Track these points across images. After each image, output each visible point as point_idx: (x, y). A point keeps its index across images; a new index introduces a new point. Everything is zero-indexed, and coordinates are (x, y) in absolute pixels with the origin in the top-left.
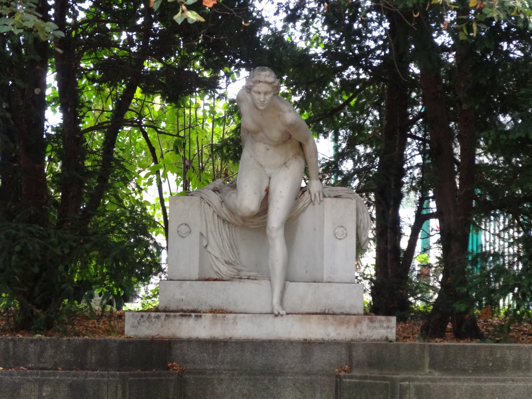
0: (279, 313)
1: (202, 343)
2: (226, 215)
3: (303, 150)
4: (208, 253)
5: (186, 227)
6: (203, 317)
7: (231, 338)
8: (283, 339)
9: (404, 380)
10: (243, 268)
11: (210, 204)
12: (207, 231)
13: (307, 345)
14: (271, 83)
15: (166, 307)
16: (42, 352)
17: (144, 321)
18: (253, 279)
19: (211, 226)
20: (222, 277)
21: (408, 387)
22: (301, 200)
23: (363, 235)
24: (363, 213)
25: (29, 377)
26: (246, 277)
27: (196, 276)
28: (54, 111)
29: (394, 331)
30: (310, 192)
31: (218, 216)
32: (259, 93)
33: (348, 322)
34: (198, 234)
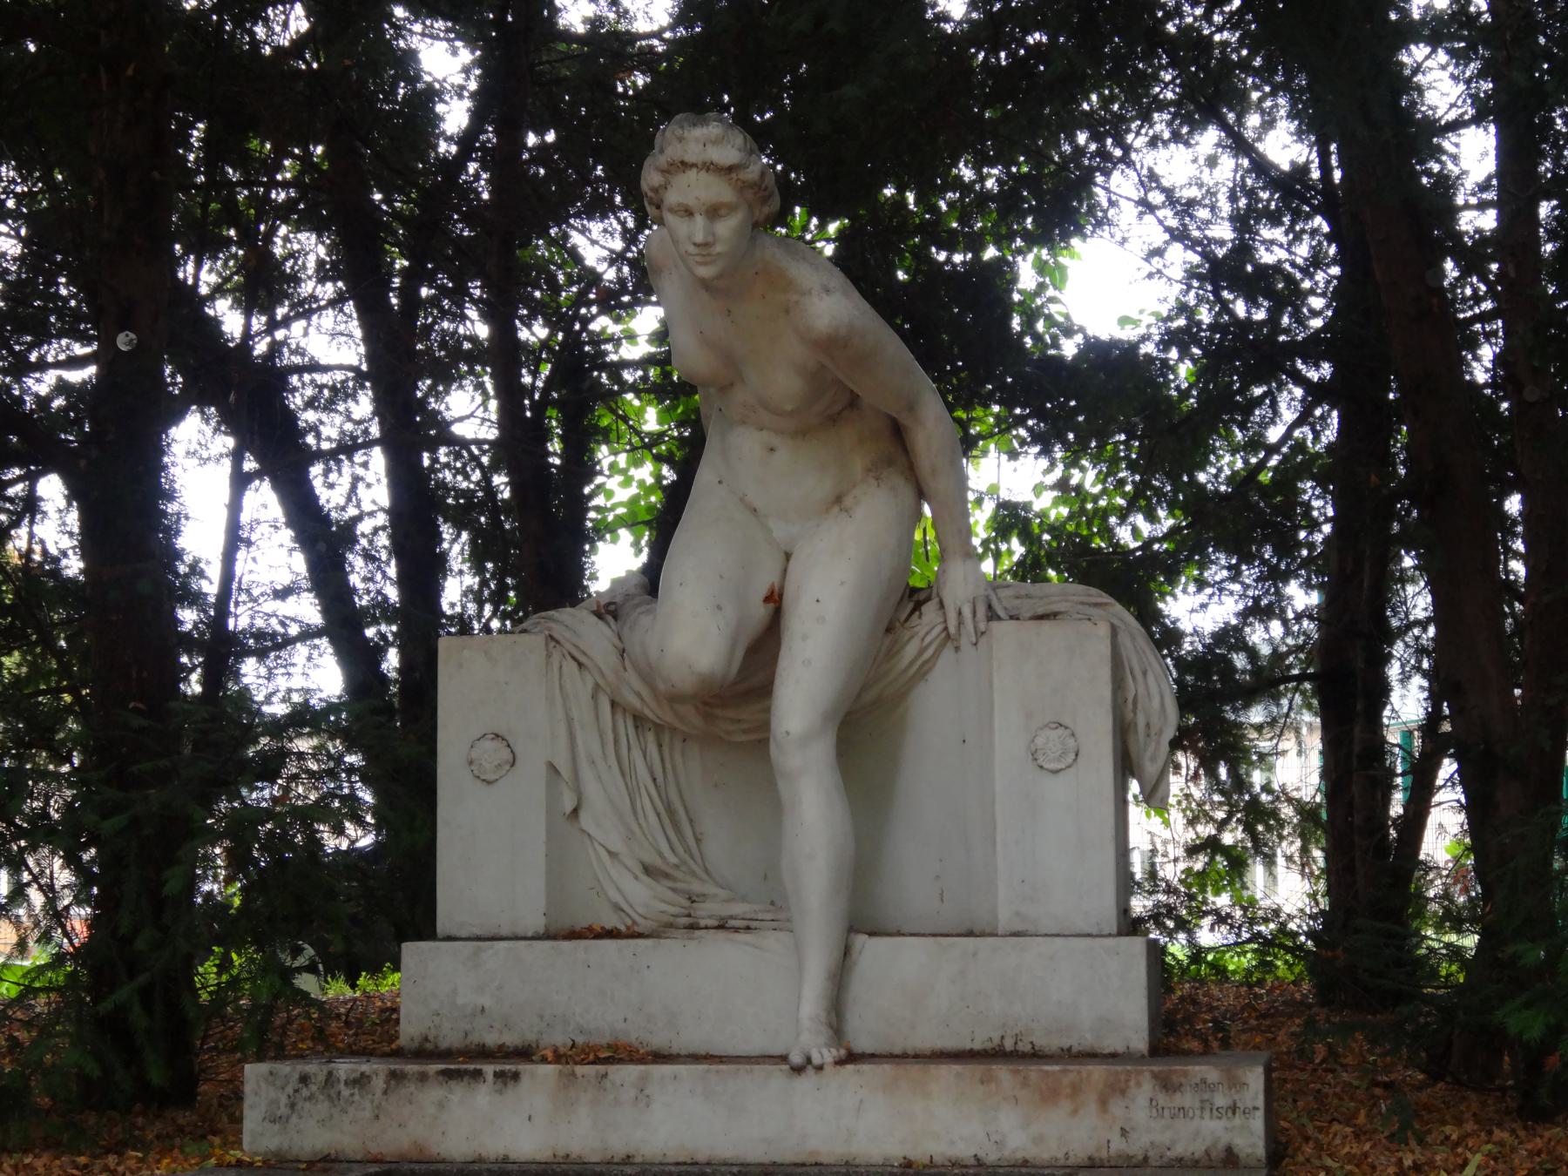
0: (809, 1060)
2: (639, 695)
6: (525, 1081)
8: (825, 1160)
10: (710, 889)
11: (582, 659)
14: (730, 169)
15: (426, 1039)
17: (310, 1098)
19: (588, 742)
20: (634, 922)
22: (908, 634)
23: (1149, 754)
24: (1145, 673)
26: (715, 923)
27: (534, 921)
28: (636, 545)
29: (1258, 1123)
30: (942, 605)
31: (614, 704)
32: (689, 213)
33: (1076, 1090)
34: (542, 770)
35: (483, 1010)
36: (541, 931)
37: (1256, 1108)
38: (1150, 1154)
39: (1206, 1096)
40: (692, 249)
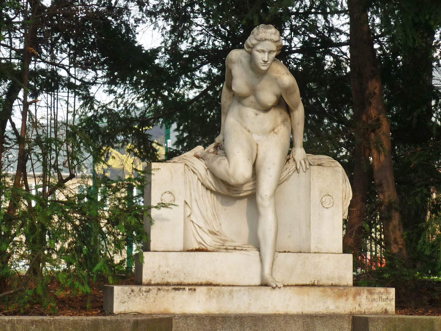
0: (277, 286)
2: (210, 181)
3: (290, 117)
4: (191, 223)
5: (169, 195)
7: (287, 314)
11: (195, 171)
14: (277, 42)
26: (233, 248)
27: (180, 246)
30: (294, 160)
32: (264, 51)
33: (347, 294)
35: (168, 272)
36: (182, 249)
37: (393, 299)
38: (366, 311)
39: (381, 296)
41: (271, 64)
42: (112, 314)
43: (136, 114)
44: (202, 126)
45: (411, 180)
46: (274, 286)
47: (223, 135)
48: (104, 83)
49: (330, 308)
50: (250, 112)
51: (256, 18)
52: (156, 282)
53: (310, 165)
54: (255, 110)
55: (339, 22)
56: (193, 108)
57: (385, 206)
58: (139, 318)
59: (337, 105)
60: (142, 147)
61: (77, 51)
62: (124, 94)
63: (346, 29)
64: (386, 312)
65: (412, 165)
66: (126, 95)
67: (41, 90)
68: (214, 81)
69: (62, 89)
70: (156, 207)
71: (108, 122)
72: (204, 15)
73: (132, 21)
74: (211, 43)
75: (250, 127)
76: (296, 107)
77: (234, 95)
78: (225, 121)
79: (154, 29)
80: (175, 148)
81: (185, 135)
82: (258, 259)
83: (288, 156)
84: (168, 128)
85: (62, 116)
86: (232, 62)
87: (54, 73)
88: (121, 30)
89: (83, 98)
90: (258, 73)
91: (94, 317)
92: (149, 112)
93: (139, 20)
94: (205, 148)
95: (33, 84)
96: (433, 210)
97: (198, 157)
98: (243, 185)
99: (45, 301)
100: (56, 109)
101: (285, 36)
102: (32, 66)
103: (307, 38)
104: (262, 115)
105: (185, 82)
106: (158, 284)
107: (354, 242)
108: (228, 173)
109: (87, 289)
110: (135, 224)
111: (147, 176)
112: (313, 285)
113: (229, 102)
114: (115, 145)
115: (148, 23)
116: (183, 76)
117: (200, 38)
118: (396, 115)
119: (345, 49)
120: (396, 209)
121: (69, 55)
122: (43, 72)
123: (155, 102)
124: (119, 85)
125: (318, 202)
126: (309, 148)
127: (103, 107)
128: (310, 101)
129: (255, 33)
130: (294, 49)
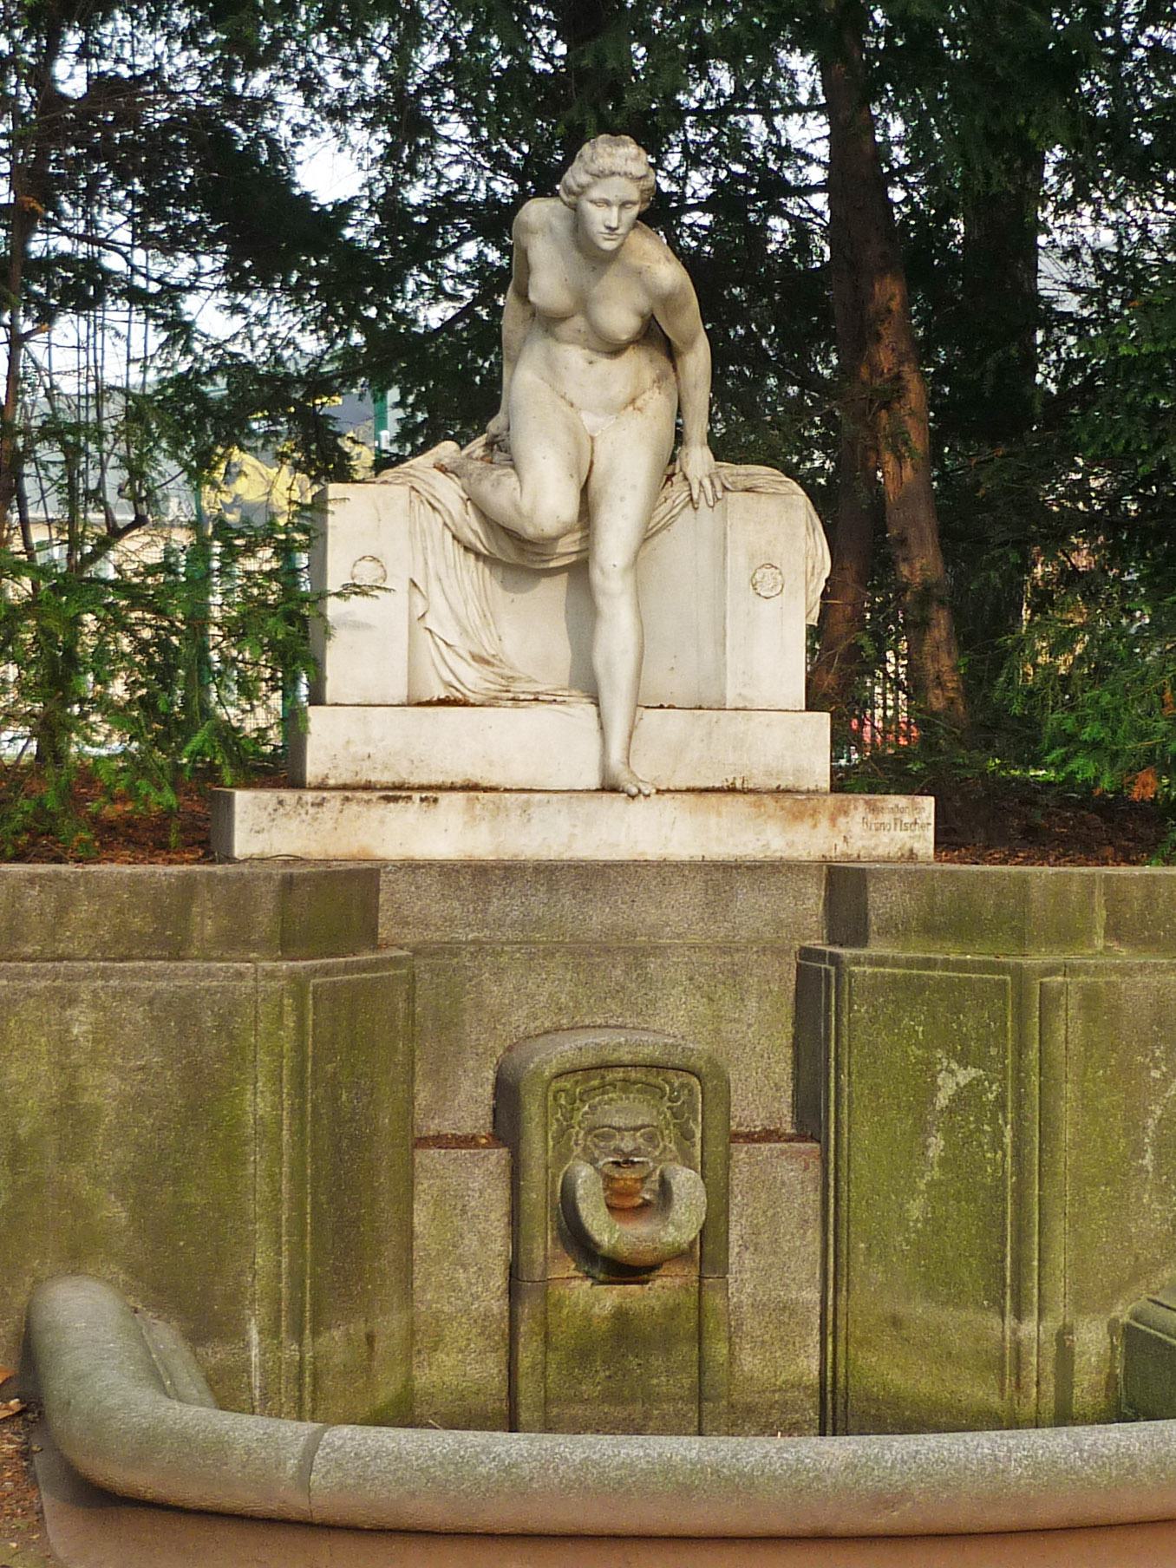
1: (448, 871)
2: (475, 532)
3: (675, 369)
5: (372, 564)
9: (1051, 971)
11: (436, 504)
12: (427, 575)
13: (722, 875)
16: (62, 909)
18: (550, 702)
21: (1063, 990)
25: (39, 985)
27: (400, 694)
30: (686, 478)
32: (607, 203)
33: (815, 811)
36: (404, 700)
40: (603, 230)
41: (626, 235)
42: (229, 859)
43: (296, 364)
44: (456, 391)
45: (987, 531)
46: (634, 791)
47: (507, 413)
48: (218, 288)
49: (773, 847)
50: (574, 356)
51: (591, 120)
52: (341, 781)
53: (725, 489)
54: (587, 351)
55: (804, 133)
56: (438, 348)
57: (1072, 651)
58: (296, 870)
59: (797, 343)
60: (313, 447)
61: (151, 206)
62: (268, 314)
63: (822, 150)
64: (912, 856)
65: (982, 492)
66: (273, 319)
67: (63, 305)
68: (491, 281)
69: (114, 303)
70: (338, 595)
71: (228, 384)
72: (464, 114)
73: (284, 132)
74: (482, 186)
75: (571, 396)
76: (690, 343)
77: (533, 315)
78: (511, 380)
79: (340, 150)
80: (394, 449)
81: (420, 417)
82: (593, 724)
83: (669, 468)
84: (379, 397)
85: (114, 372)
86: (527, 229)
87: (92, 264)
88: (258, 156)
89: (166, 326)
90: (593, 256)
91: (185, 868)
92: (331, 360)
93: (304, 128)
94: (462, 447)
95: (43, 291)
96: (1037, 605)
97: (443, 469)
98: (556, 539)
99: (66, 825)
100: (95, 356)
101: (670, 169)
102: (37, 246)
103: (723, 174)
104: (604, 364)
105: (419, 285)
106: (344, 787)
107: (835, 679)
108: (520, 513)
109: (169, 798)
110: (291, 636)
111: (316, 516)
112: (732, 790)
113: (521, 331)
114: (246, 443)
115: (329, 134)
116: (415, 271)
117: (455, 172)
118: (948, 366)
119: (819, 201)
120: (941, 602)
121: (131, 217)
122: (65, 260)
123: (345, 334)
124: (254, 293)
125: (745, 581)
126: (722, 449)
127: (217, 346)
128: (732, 334)
129: (587, 157)
130: (690, 201)
